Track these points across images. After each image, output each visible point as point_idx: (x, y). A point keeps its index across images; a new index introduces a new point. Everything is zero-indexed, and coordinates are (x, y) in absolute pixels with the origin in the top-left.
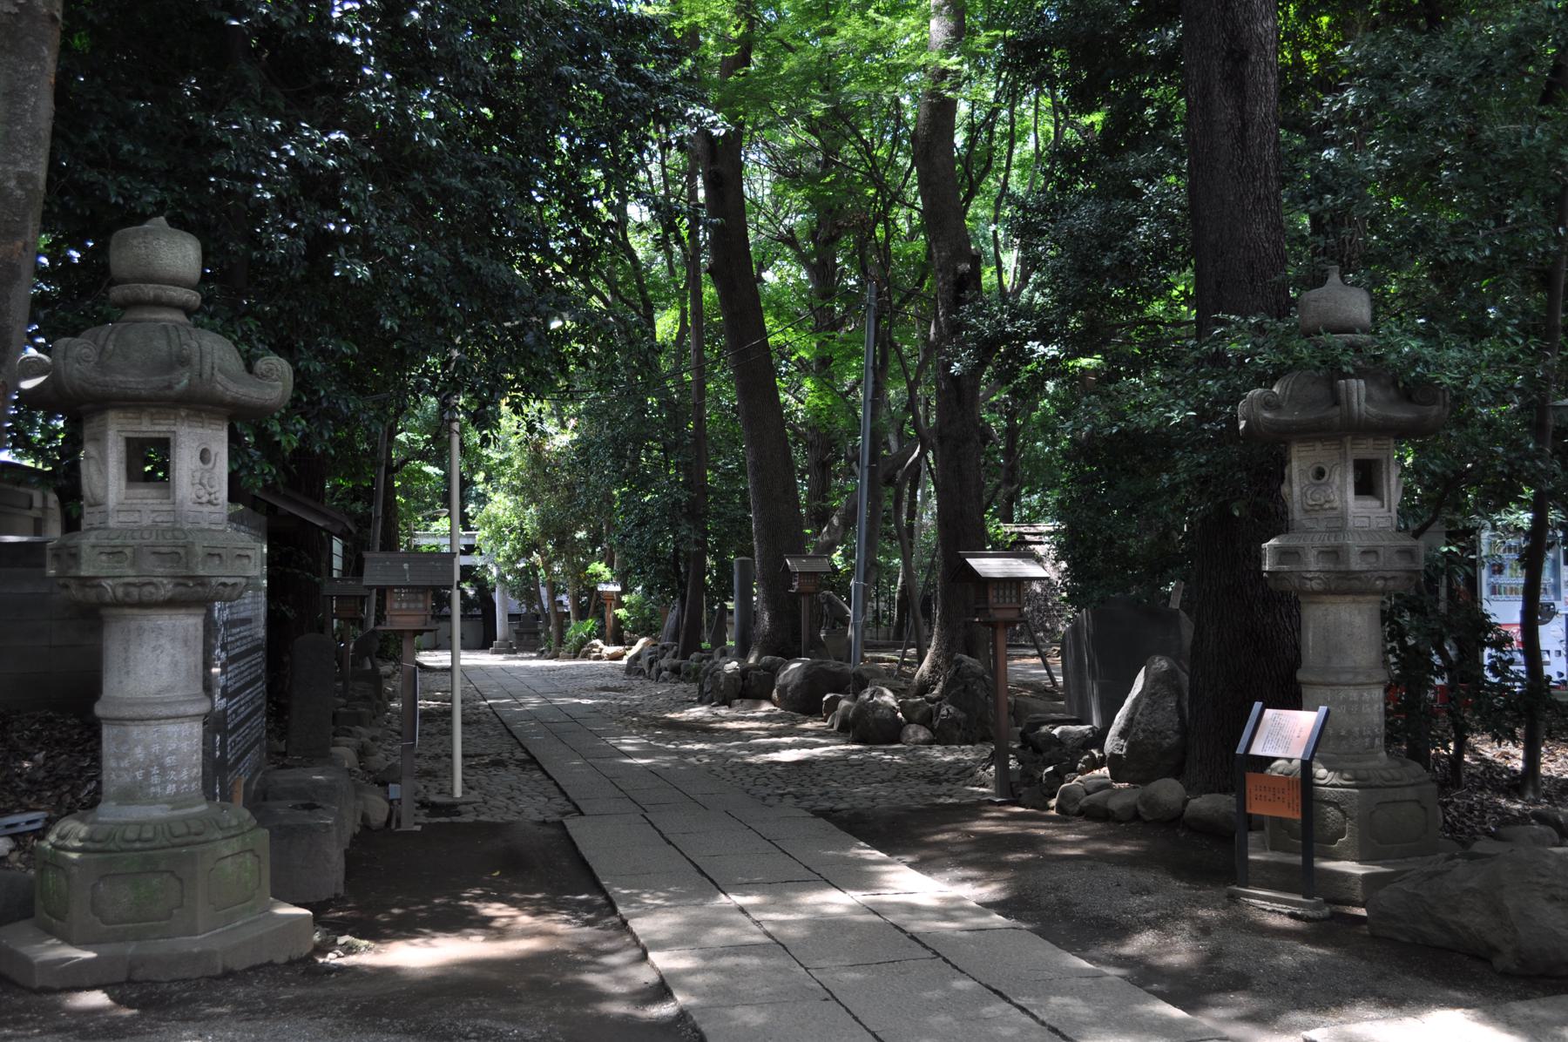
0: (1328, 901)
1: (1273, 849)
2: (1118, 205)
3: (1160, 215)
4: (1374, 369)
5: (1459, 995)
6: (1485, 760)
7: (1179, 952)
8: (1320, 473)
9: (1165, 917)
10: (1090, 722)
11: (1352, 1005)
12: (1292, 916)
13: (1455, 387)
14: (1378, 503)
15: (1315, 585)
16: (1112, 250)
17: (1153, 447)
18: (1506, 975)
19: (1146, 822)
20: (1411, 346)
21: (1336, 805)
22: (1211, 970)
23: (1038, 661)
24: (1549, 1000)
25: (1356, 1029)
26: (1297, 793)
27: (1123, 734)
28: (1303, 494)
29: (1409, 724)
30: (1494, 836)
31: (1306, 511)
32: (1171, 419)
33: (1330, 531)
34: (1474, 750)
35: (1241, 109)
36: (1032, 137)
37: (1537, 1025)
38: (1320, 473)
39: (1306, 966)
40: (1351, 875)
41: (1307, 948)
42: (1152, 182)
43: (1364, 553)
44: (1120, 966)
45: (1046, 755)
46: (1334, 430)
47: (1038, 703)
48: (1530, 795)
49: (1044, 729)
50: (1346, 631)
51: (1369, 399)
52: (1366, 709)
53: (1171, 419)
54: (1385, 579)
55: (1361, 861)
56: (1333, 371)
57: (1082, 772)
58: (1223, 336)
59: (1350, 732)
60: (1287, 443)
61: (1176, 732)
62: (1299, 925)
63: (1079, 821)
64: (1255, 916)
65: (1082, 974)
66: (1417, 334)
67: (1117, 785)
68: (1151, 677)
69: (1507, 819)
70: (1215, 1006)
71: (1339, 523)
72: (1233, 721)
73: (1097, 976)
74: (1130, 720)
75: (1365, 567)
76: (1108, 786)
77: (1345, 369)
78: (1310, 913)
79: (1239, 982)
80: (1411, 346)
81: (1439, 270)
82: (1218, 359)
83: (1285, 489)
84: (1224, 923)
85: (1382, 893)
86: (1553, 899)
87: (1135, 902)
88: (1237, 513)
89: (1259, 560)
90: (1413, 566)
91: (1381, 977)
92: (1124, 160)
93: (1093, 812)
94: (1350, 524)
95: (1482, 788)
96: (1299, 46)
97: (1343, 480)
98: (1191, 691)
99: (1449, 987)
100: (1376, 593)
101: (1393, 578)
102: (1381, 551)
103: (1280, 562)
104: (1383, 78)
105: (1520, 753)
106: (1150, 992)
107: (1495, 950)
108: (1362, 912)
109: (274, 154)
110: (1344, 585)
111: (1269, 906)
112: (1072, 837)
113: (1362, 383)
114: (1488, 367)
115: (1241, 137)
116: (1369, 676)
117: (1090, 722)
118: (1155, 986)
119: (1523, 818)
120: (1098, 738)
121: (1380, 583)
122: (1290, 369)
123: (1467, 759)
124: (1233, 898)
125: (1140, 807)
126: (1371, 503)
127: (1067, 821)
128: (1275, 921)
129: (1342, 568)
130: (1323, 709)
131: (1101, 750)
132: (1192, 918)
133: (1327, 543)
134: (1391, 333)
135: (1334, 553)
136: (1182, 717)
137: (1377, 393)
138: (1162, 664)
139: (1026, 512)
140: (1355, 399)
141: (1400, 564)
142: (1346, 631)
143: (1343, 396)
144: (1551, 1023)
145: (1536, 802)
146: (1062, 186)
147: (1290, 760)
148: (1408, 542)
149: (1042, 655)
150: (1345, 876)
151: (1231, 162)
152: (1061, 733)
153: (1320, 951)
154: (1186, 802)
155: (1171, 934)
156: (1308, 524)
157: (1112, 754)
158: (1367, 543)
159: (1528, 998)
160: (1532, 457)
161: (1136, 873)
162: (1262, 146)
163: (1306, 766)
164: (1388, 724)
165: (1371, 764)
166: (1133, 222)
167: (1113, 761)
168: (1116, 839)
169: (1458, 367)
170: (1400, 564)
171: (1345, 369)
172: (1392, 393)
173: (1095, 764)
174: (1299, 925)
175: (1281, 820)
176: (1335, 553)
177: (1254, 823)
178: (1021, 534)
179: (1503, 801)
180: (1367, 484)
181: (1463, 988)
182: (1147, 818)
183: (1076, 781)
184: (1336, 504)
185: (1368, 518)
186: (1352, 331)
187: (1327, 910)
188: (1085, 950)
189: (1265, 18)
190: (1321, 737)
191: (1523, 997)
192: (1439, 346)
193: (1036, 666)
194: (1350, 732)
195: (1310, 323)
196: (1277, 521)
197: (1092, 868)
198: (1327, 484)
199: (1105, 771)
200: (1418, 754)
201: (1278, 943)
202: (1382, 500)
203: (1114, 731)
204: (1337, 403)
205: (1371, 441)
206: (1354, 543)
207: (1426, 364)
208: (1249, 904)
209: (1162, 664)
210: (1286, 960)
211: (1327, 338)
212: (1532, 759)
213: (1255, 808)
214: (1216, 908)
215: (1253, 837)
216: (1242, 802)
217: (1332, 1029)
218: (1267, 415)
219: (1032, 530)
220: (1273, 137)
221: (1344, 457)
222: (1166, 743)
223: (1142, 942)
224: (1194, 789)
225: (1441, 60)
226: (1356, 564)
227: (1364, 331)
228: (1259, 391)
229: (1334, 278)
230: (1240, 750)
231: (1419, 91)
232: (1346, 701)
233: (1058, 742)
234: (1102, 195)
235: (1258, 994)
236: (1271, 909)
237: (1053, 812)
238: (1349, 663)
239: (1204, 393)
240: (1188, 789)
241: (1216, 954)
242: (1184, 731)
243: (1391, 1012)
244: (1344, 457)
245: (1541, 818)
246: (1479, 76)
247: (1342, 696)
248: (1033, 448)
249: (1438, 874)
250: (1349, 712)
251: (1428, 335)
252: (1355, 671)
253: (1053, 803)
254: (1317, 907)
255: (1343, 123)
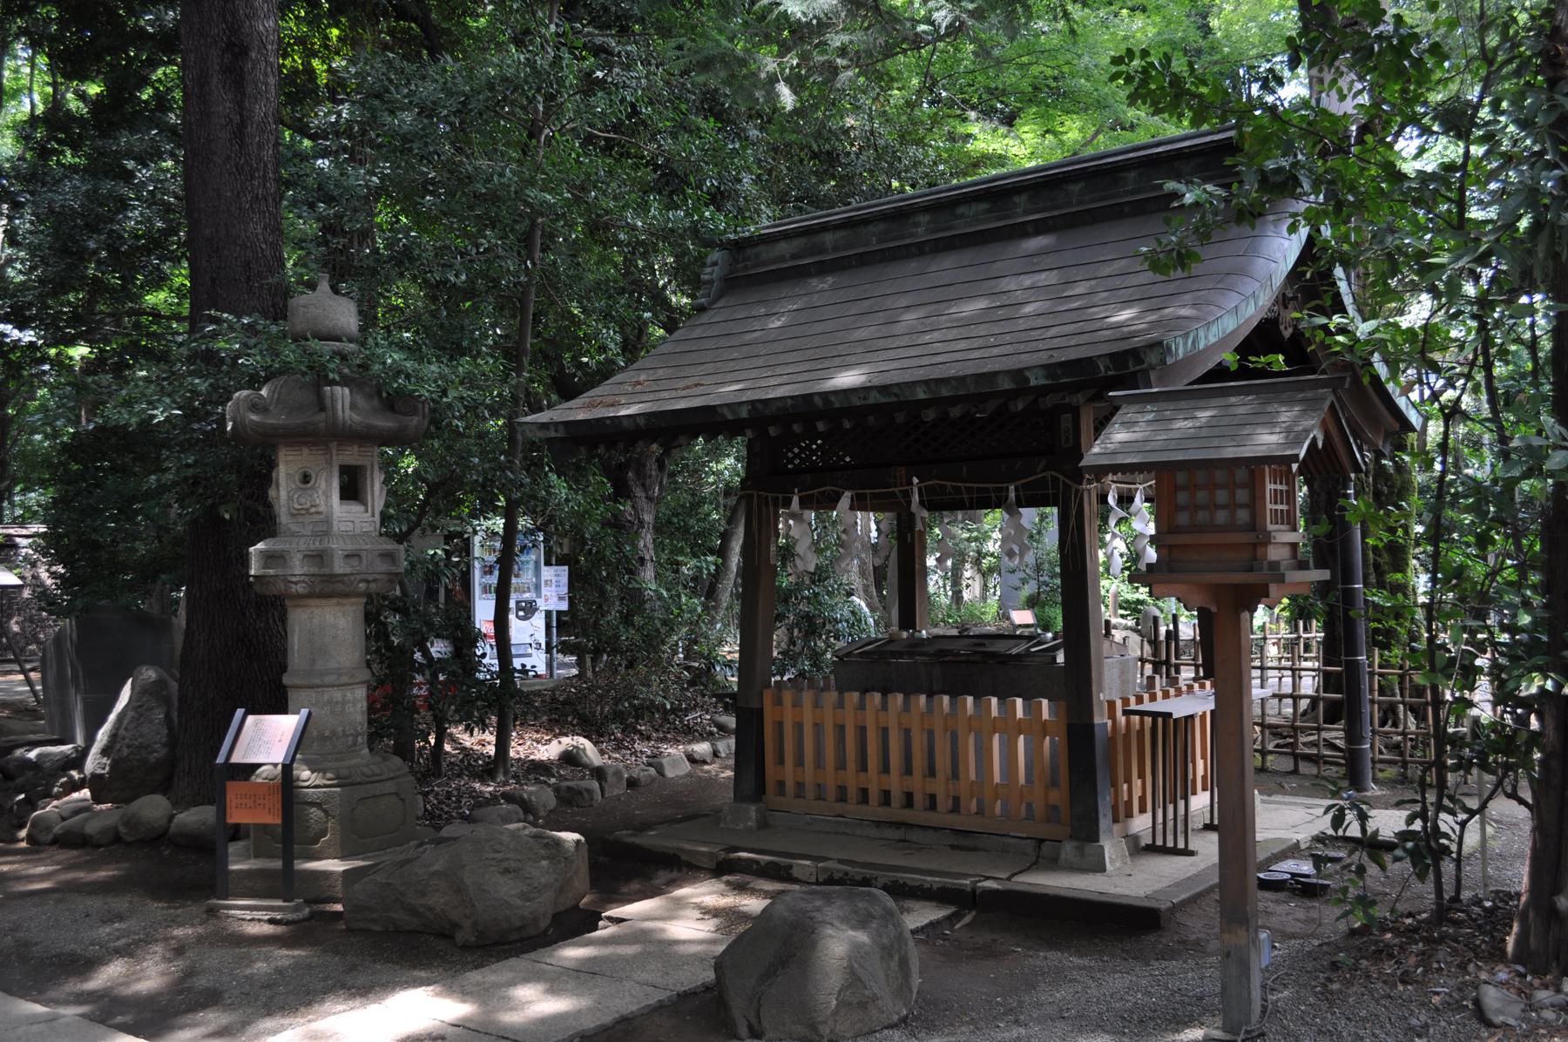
0: (308, 902)
1: (256, 857)
2: (107, 186)
3: (152, 201)
4: (360, 379)
5: (423, 974)
6: (465, 748)
7: (148, 978)
8: (306, 478)
9: (137, 943)
10: (72, 741)
11: (323, 1001)
12: (271, 921)
13: (433, 400)
14: (362, 508)
15: (300, 589)
16: (99, 232)
17: (134, 446)
18: (466, 947)
19: (129, 844)
20: (393, 357)
21: (318, 805)
22: (180, 992)
23: (21, 677)
24: (500, 964)
25: (322, 1025)
26: (278, 797)
27: (105, 752)
28: (290, 498)
29: (392, 718)
30: (468, 819)
31: (293, 515)
32: (155, 416)
33: (315, 535)
34: (454, 740)
35: (240, 104)
36: (27, 101)
37: (487, 990)
38: (306, 478)
39: (280, 971)
40: (331, 873)
41: (284, 952)
42: (145, 166)
43: (348, 556)
44: (80, 1003)
45: (18, 781)
46: (322, 435)
47: (17, 725)
48: (501, 778)
49: (19, 752)
50: (328, 635)
51: (353, 406)
52: (349, 708)
53: (155, 416)
54: (368, 582)
55: (343, 858)
56: (320, 378)
57: (58, 797)
58: (214, 335)
59: (333, 733)
60: (274, 448)
61: (165, 745)
62: (279, 929)
63: (52, 850)
64: (234, 927)
65: (34, 1020)
66: (401, 346)
67: (99, 807)
68: (137, 689)
69: (481, 802)
70: (182, 1028)
71: (324, 528)
72: (217, 728)
73: (51, 1019)
74: (114, 736)
75: (348, 570)
76: (87, 809)
77: (331, 376)
78: (289, 916)
79: (212, 999)
80: (393, 357)
81: (435, 290)
82: (210, 357)
83: (272, 493)
84: (200, 940)
85: (357, 887)
86: (507, 871)
87: (105, 931)
88: (227, 516)
89: (245, 561)
90: (393, 569)
91: (353, 968)
92: (116, 138)
93: (71, 840)
94: (335, 528)
95: (459, 776)
96: (310, 53)
97: (329, 484)
98: (180, 700)
99: (414, 967)
100: (359, 595)
101: (375, 580)
102: (364, 554)
103: (266, 566)
104: (376, 98)
105: (493, 739)
106: (110, 1026)
107: (456, 926)
108: (339, 907)
109: (640, 263)
110: (328, 588)
111: (248, 915)
112: (41, 869)
113: (347, 390)
114: (462, 383)
115: (240, 132)
116: (352, 676)
117: (72, 741)
118: (119, 1019)
119: (494, 799)
120: (78, 761)
121: (362, 586)
122: (280, 373)
123: (447, 748)
124: (212, 912)
125: (122, 829)
126: (356, 508)
127: (38, 852)
128: (253, 929)
129: (326, 571)
130: (304, 712)
131: (81, 771)
132: (166, 939)
133: (312, 547)
134: (377, 344)
135: (319, 557)
136: (170, 729)
137: (361, 401)
138: (150, 674)
139: (19, 512)
140: (339, 406)
141: (382, 567)
142: (328, 635)
143: (328, 402)
144: (498, 986)
145: (506, 784)
146: (44, 153)
147: (275, 765)
148: (390, 546)
149: (23, 672)
150: (326, 875)
151: (229, 158)
152: (39, 756)
153: (296, 953)
154: (172, 817)
155: (140, 961)
156: (294, 528)
157: (94, 775)
158: (350, 547)
159: (482, 966)
160: (502, 468)
161: (109, 900)
162: (260, 146)
163: (287, 768)
164: (370, 722)
165: (354, 762)
166: (123, 205)
167: (94, 782)
168: (91, 866)
169: (435, 381)
170: (382, 567)
171: (331, 376)
172: (376, 402)
173: (75, 786)
174: (279, 929)
175: (265, 825)
176: (319, 557)
177: (236, 833)
178: (9, 536)
179: (477, 785)
180: (352, 490)
181: (427, 966)
182: (129, 839)
183: (51, 808)
184: (322, 508)
185: (353, 522)
186: (338, 339)
187: (307, 910)
188: (41, 992)
189: (267, 17)
190: (301, 741)
191: (478, 966)
192: (420, 360)
193: (20, 683)
194: (333, 733)
195: (299, 328)
196: (265, 524)
197: (59, 901)
198: (313, 488)
199: (85, 793)
200: (404, 751)
201: (254, 951)
202: (365, 505)
203: (95, 749)
204: (322, 409)
205: (356, 448)
206: (338, 547)
207: (408, 376)
208: (228, 916)
209: (150, 674)
210: (261, 967)
211: (315, 344)
212: (502, 744)
213: (235, 817)
214: (192, 925)
215: (233, 848)
216: (222, 812)
217: (299, 1030)
218: (254, 417)
219: (24, 532)
220: (272, 138)
221: (330, 463)
222: (153, 757)
223: (110, 973)
224: (180, 804)
225: (427, 90)
226: (339, 567)
227: (351, 341)
228: (245, 393)
229: (324, 286)
230: (220, 760)
231: (408, 117)
232: (329, 702)
233: (34, 766)
234: (94, 170)
235: (230, 1007)
236: (251, 917)
237: (24, 845)
238: (333, 665)
239: (191, 391)
240: (175, 804)
241: (189, 974)
242: (172, 743)
243: (358, 1002)
244: (330, 463)
245: (509, 798)
246: (459, 111)
247: (326, 697)
248: (29, 442)
249: (408, 861)
250: (332, 712)
251: (412, 350)
252: (338, 672)
253: (23, 833)
254: (296, 909)
255: (337, 134)
